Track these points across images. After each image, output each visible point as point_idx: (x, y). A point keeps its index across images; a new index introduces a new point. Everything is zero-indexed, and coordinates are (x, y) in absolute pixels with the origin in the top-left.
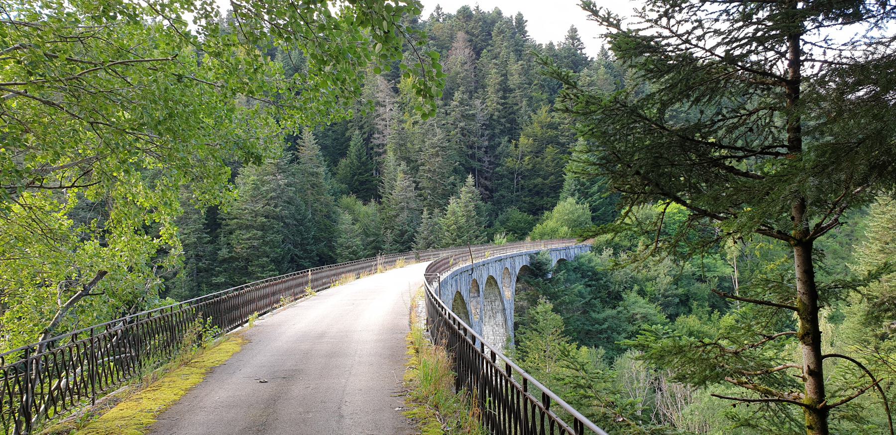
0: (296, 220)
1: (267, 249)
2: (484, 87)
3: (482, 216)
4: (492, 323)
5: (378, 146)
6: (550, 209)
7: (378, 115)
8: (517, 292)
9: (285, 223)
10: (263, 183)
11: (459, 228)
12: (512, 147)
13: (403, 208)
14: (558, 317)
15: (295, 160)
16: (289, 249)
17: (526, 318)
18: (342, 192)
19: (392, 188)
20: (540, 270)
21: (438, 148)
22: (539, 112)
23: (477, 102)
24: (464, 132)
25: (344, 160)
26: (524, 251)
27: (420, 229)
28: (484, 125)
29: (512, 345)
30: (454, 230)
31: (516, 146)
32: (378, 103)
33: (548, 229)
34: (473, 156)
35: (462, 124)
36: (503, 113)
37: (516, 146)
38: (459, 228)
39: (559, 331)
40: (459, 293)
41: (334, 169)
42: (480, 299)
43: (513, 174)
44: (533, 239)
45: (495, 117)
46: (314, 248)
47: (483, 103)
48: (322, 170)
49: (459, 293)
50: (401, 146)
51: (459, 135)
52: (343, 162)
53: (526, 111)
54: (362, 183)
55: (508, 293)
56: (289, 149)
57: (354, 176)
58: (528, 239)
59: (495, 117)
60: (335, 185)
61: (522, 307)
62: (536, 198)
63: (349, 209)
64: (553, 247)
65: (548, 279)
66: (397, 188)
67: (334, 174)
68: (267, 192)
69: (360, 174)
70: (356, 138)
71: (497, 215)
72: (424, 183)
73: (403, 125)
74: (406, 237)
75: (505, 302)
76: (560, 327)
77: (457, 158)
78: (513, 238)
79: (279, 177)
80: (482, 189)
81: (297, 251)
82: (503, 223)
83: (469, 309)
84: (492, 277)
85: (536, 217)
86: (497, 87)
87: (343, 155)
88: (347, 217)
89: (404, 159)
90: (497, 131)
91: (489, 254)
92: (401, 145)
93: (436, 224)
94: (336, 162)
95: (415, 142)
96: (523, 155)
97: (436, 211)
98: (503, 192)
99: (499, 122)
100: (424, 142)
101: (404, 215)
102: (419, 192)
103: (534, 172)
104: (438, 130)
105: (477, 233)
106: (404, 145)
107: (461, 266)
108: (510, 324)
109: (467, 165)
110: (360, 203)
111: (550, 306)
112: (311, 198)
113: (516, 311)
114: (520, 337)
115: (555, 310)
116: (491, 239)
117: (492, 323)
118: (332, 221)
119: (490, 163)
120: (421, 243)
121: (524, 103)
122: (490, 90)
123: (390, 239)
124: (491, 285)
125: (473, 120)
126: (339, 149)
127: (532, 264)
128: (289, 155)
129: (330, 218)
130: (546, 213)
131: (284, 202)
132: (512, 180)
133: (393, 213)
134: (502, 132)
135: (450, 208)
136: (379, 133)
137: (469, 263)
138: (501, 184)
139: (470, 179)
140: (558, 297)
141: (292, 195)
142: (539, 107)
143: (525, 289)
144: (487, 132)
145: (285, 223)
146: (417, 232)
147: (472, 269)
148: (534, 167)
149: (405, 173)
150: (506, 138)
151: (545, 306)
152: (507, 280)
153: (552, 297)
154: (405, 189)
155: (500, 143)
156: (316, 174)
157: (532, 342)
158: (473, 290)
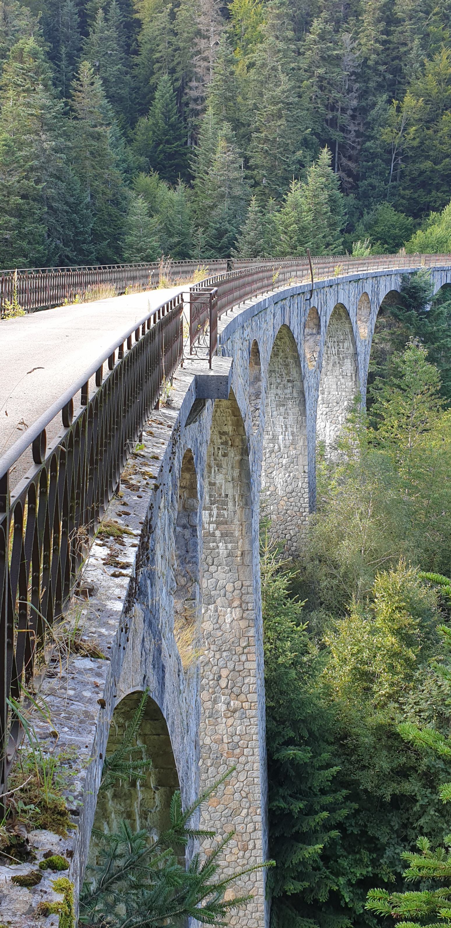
0: (67, 203)
1: (24, 244)
2: (357, 14)
3: (338, 214)
4: (337, 373)
5: (196, 100)
6: (439, 209)
7: (199, 52)
8: (378, 329)
9: (50, 207)
10: (21, 145)
11: (302, 229)
12: (392, 111)
13: (222, 196)
14: (434, 369)
15: (68, 112)
16: (57, 247)
17: (387, 367)
18: (141, 169)
19: (209, 163)
20: (415, 298)
21: (281, 105)
22: (437, 57)
23: (346, 37)
24: (323, 84)
25: (146, 120)
26: (394, 268)
27: (244, 228)
28: (353, 73)
29: (362, 407)
30: (294, 231)
31: (399, 109)
32: (198, 33)
33: (433, 239)
34: (333, 123)
35: (321, 71)
36: (383, 56)
37: (399, 109)
38: (302, 229)
39: (433, 390)
40: (286, 328)
41: (130, 133)
42: (321, 338)
43: (390, 152)
44: (410, 252)
45: (370, 63)
46: (92, 247)
47: (353, 39)
48: (109, 132)
49: (286, 328)
50: (228, 99)
51: (315, 88)
52: (144, 122)
53: (418, 56)
54: (170, 156)
55: (364, 330)
56: (58, 97)
57: (158, 145)
58: (403, 251)
59: (370, 63)
60: (131, 157)
61: (383, 351)
62: (421, 192)
63: (149, 195)
64: (438, 265)
65: (424, 313)
66: (216, 164)
67: (130, 141)
68: (27, 159)
69: (168, 142)
70: (164, 83)
71: (362, 215)
72: (257, 159)
73: (233, 68)
74: (225, 240)
75: (358, 344)
76: (434, 385)
77: (310, 123)
78: (381, 250)
79: (44, 137)
80: (343, 175)
81: (68, 251)
82: (369, 227)
83: (301, 352)
84: (342, 306)
85: (418, 220)
86: (378, 14)
87: (144, 111)
88: (140, 205)
89: (228, 119)
90: (372, 84)
91: (340, 270)
92: (227, 99)
93: (270, 222)
94: (133, 123)
95: (250, 95)
96: (408, 125)
97: (271, 201)
98: (374, 180)
99: (376, 70)
100: (261, 94)
101: (225, 206)
102: (249, 172)
103: (421, 151)
104: (283, 77)
105: (329, 239)
106: (233, 98)
107: (293, 285)
108: (363, 375)
109: (324, 136)
110: (164, 185)
111: (423, 352)
112: (90, 173)
113: (373, 357)
114: (376, 395)
115: (431, 359)
116: (348, 249)
117: (337, 373)
118: (121, 209)
119: (358, 134)
120: (245, 249)
121: (416, 42)
122: (367, 18)
123: (202, 243)
124: (340, 317)
125: (338, 66)
126: (140, 104)
127: (404, 289)
128: (60, 104)
129: (118, 202)
130: (433, 215)
131: (51, 175)
132: (388, 162)
133: (209, 202)
134: (380, 87)
135: (290, 198)
136: (198, 80)
137: (306, 281)
138: (371, 168)
139: (325, 155)
140: (437, 339)
141: (61, 165)
142: (438, 49)
143: (390, 326)
144: (357, 85)
145: (50, 207)
146: (241, 233)
147: (311, 291)
148: (422, 143)
149: (228, 140)
150: (385, 97)
151: (416, 352)
152: (365, 312)
153: (428, 339)
154: (227, 166)
155: (374, 104)
156: (98, 137)
157: (393, 404)
158: (312, 324)
